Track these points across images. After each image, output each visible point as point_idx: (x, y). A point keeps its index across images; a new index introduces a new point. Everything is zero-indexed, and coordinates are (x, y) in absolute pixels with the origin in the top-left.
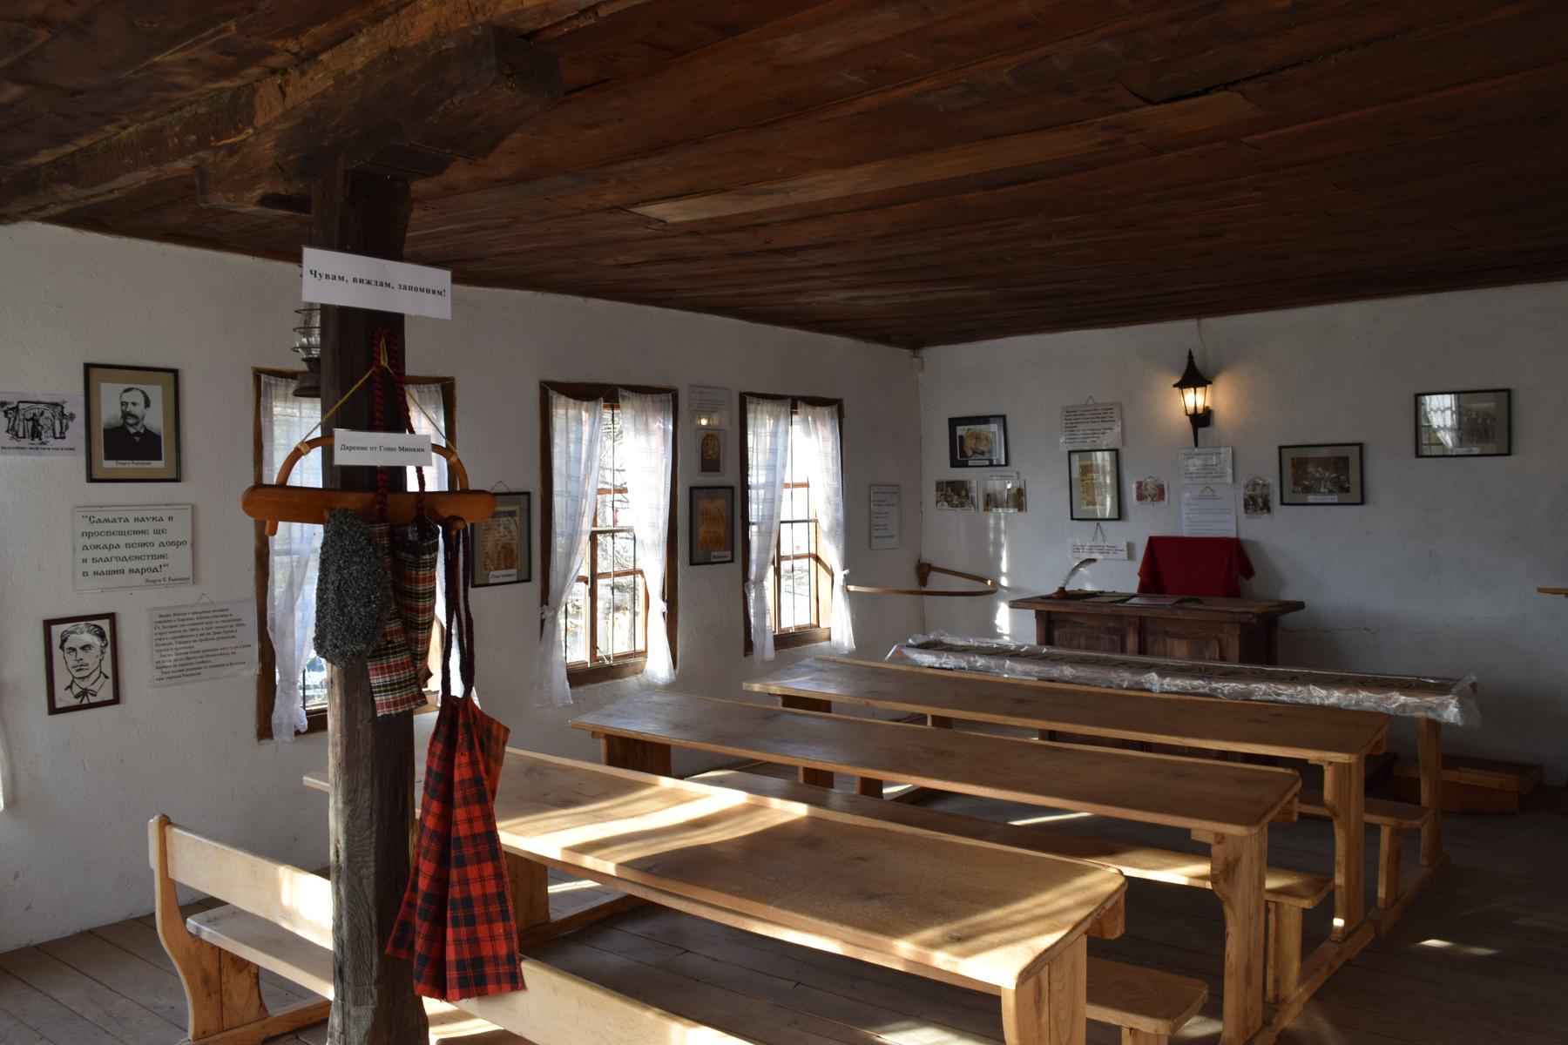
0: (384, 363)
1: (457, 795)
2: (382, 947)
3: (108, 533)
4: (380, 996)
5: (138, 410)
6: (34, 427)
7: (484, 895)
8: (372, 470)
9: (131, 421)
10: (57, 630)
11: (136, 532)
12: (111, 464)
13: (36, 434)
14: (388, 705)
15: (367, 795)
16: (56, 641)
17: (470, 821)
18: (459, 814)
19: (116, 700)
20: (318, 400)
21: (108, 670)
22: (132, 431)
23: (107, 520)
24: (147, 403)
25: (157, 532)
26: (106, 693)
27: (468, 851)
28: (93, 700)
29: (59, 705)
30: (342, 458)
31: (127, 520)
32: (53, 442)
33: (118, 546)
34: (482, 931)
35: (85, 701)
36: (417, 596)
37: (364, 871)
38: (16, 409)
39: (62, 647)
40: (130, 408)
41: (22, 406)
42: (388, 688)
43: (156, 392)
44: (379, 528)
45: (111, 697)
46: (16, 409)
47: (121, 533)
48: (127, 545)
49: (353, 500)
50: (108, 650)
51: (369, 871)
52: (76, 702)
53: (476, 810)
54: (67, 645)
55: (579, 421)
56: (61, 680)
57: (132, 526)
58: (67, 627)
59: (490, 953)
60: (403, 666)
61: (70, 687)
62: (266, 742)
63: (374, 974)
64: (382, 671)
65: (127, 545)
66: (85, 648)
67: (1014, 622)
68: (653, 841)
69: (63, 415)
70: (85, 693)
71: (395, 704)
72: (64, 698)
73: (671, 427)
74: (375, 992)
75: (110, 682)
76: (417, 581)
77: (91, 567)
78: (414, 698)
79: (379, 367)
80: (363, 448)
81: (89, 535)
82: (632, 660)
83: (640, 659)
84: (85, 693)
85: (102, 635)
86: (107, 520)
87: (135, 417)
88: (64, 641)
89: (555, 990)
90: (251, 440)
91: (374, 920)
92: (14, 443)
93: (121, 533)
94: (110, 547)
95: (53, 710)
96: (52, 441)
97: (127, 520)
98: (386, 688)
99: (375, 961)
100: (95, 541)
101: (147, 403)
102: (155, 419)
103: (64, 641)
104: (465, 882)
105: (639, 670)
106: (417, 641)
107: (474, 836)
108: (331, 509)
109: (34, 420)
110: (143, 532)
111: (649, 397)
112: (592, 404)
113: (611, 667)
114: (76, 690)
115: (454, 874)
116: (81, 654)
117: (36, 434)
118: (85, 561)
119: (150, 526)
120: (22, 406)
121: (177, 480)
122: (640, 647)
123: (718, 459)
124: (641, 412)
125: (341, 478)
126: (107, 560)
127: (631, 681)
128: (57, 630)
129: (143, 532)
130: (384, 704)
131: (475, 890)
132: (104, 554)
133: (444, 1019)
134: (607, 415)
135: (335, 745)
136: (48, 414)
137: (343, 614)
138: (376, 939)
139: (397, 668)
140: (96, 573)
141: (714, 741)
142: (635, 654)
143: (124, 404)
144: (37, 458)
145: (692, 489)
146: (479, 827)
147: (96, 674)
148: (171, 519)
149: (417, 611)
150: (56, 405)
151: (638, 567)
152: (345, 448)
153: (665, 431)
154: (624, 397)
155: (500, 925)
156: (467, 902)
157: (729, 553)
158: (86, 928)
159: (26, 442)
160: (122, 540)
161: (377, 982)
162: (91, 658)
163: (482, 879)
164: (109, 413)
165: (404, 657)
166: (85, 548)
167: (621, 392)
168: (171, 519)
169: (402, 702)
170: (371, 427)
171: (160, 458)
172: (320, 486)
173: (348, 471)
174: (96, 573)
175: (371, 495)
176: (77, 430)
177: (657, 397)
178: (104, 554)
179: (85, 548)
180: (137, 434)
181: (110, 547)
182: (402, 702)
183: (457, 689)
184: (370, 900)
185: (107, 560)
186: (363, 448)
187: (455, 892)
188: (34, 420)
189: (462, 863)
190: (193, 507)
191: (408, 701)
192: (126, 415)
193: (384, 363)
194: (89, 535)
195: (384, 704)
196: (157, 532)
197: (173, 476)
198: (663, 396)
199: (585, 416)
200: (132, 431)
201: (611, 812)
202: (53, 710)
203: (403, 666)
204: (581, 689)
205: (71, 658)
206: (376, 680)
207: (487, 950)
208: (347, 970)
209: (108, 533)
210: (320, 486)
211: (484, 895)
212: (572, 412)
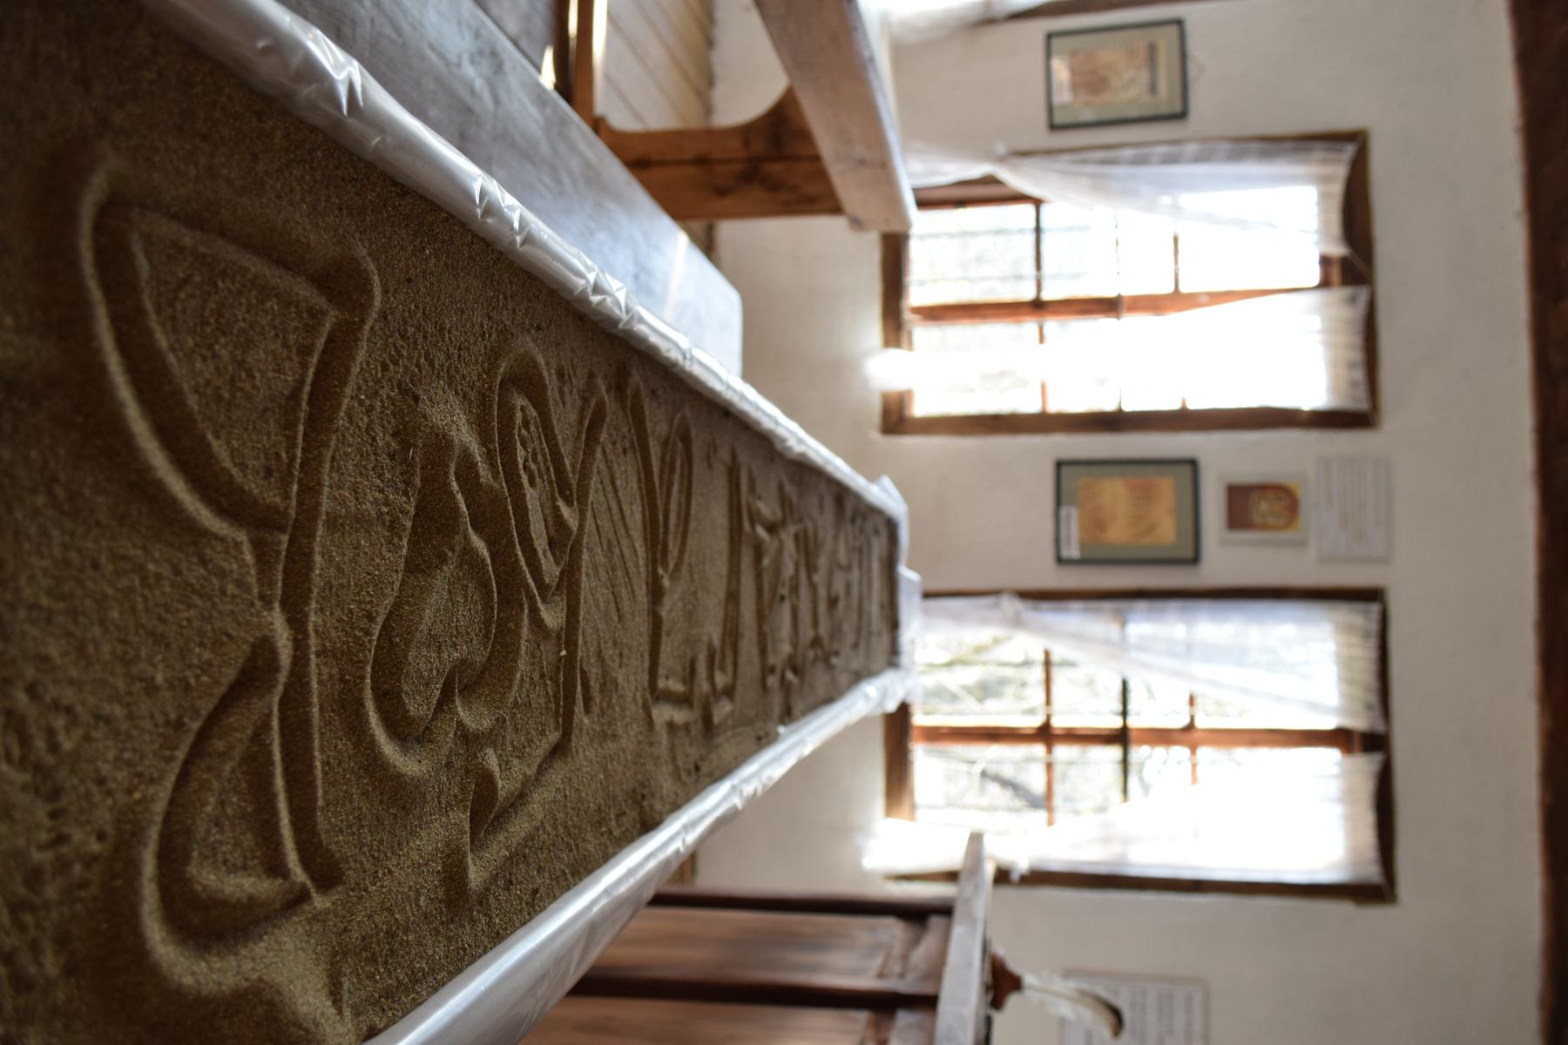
154: (1352, 300)
167: (1363, 294)
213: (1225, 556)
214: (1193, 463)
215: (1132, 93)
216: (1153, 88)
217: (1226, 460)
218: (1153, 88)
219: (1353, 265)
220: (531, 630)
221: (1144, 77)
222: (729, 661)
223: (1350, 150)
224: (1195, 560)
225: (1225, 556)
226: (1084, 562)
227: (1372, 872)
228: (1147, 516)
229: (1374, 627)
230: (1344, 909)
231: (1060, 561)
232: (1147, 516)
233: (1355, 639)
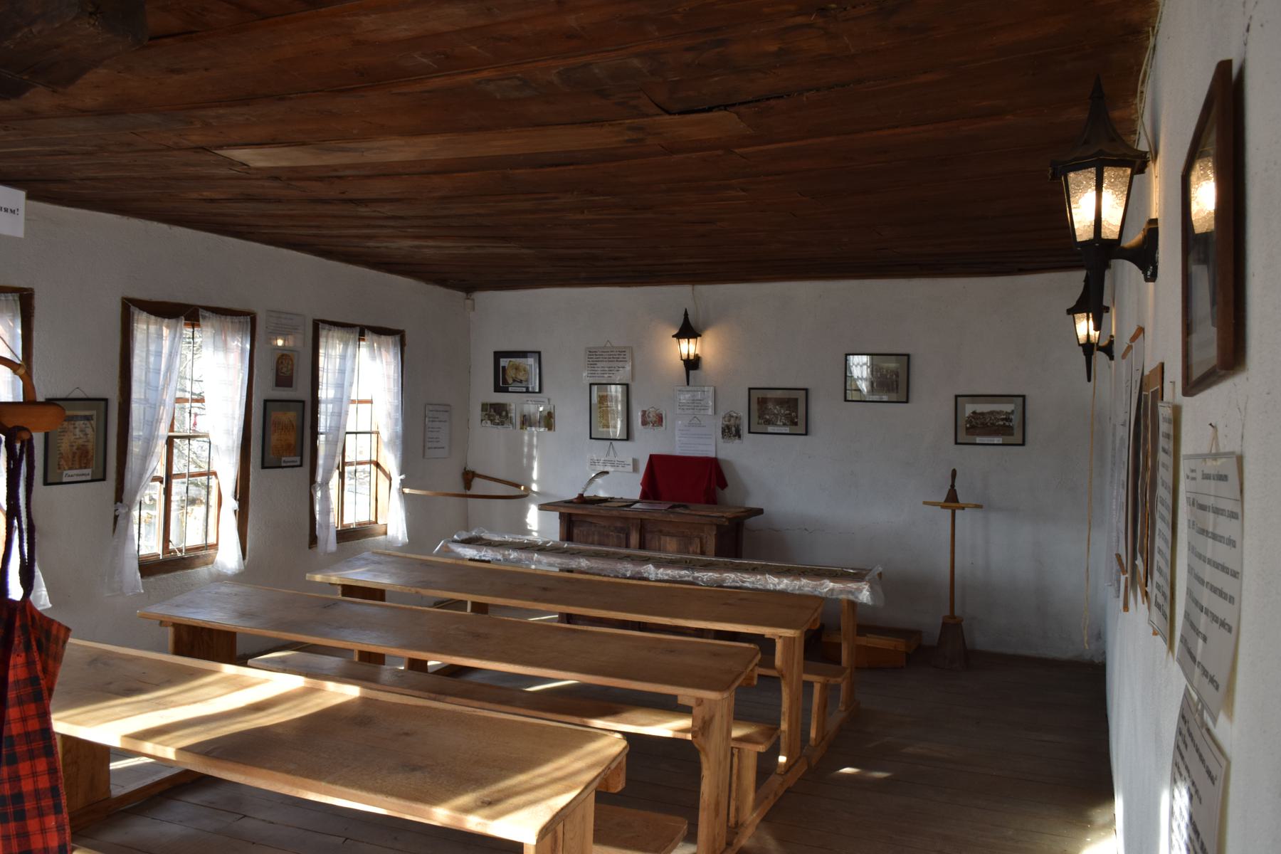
27: (21, 749)
53: (31, 709)
55: (160, 336)
73: (248, 346)
82: (203, 552)
83: (211, 552)
105: (209, 561)
107: (27, 734)
111: (229, 318)
112: (173, 321)
113: (182, 558)
127: (202, 572)
134: (188, 331)
141: (277, 628)
142: (207, 547)
146: (34, 725)
153: (243, 350)
154: (204, 317)
157: (298, 459)
163: (34, 774)
167: (201, 312)
177: (236, 319)
199: (166, 332)
204: (152, 579)
212: (153, 328)
213: (300, 391)
214: (266, 401)
215: (89, 431)
216: (88, 418)
217: (267, 389)
218: (88, 418)
219: (186, 313)
220: (270, 639)
221: (80, 423)
222: (1118, 442)
223: (133, 308)
224: (303, 402)
225: (300, 391)
226: (302, 456)
227: (398, 338)
228: (284, 432)
229: (327, 326)
230: (406, 348)
231: (301, 466)
232: (284, 432)
233: (330, 341)
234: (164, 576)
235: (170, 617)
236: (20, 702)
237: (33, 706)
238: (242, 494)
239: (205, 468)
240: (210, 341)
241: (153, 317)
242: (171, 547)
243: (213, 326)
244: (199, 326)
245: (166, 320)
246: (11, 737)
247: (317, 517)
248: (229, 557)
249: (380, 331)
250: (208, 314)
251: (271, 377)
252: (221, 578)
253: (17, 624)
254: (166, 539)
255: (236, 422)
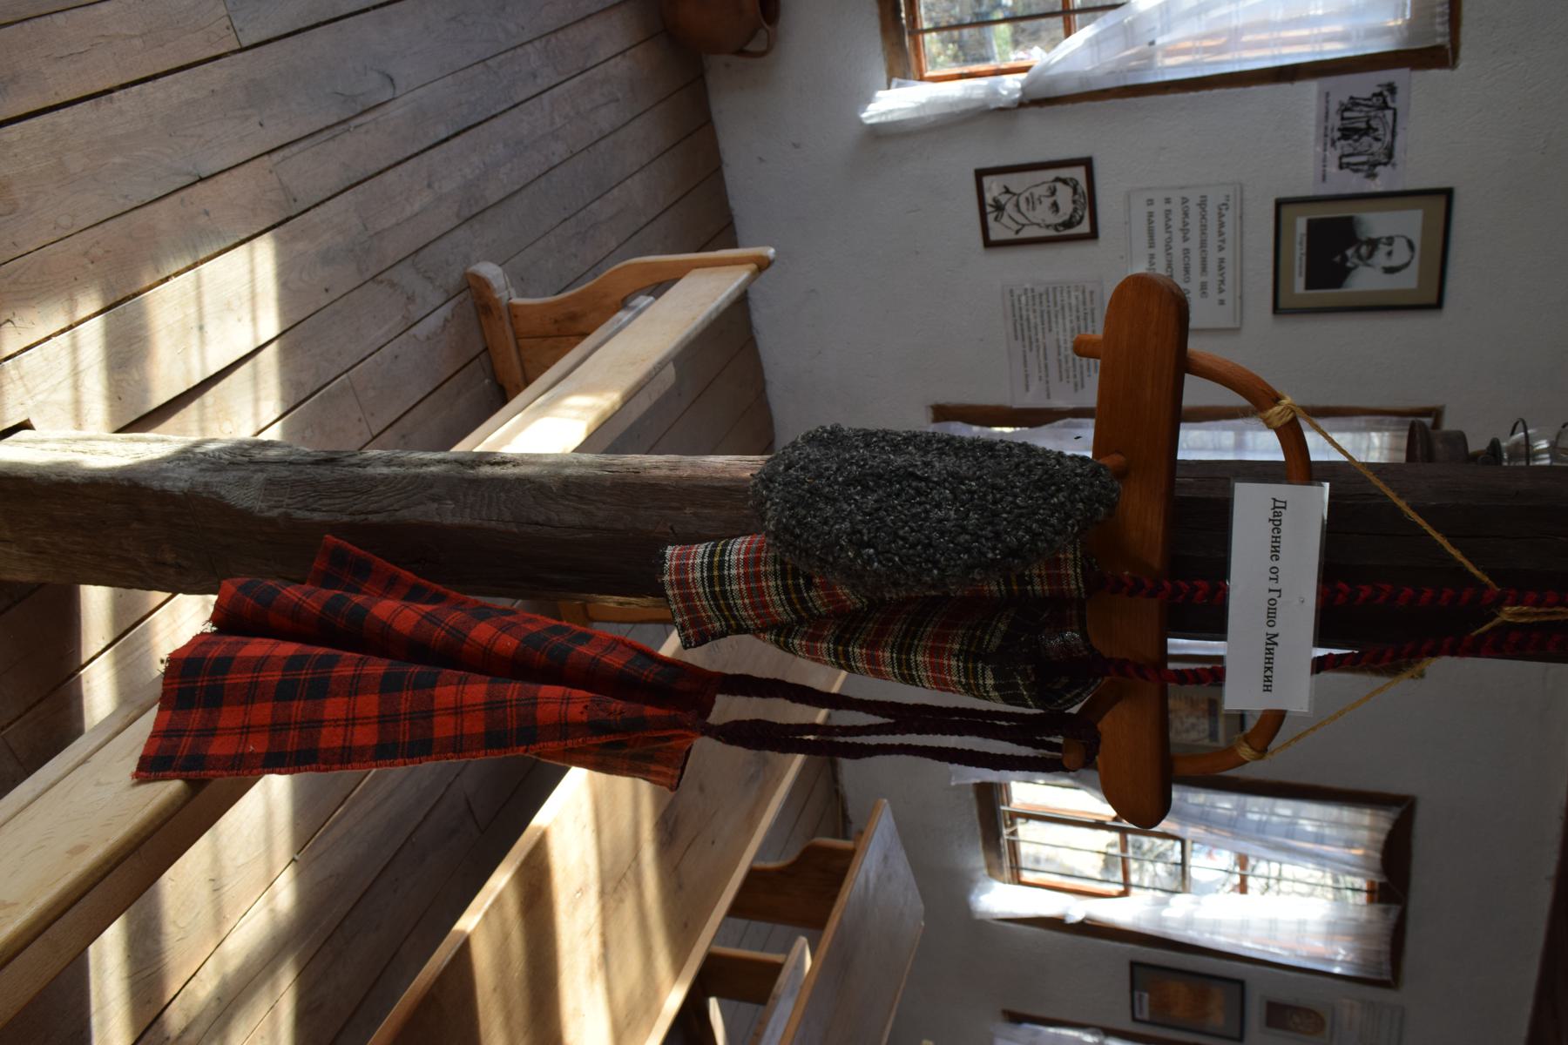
0: (1507, 613)
1: (513, 690)
2: (334, 528)
3: (1204, 228)
4: (271, 521)
5: (1380, 258)
6: (1356, 131)
7: (320, 723)
8: (1220, 568)
9: (1364, 250)
10: (1079, 173)
11: (1204, 261)
12: (1301, 226)
13: (1347, 133)
14: (681, 569)
15: (570, 518)
16: (1065, 173)
17: (458, 710)
18: (478, 690)
19: (989, 244)
20: (1401, 457)
21: (1027, 233)
22: (1350, 252)
23: (1222, 225)
24: (1390, 270)
25: (1204, 286)
26: (997, 233)
27: (405, 701)
28: (991, 218)
29: (987, 180)
30: (1249, 501)
31: (1221, 249)
32: (1333, 155)
33: (1185, 239)
34: (262, 712)
35: (989, 209)
36: (904, 649)
37: (450, 505)
38: (1385, 106)
39: (1058, 179)
40: (1383, 249)
41: (1389, 114)
42: (716, 570)
43: (1407, 281)
44: (1073, 580)
45: (993, 236)
46: (1385, 106)
47: (1203, 244)
48: (1186, 251)
49: (1144, 520)
50: (1051, 233)
51: (449, 515)
52: (989, 198)
53: (475, 725)
54: (1059, 185)
55: (1349, 844)
56: (1016, 181)
57: (1213, 257)
58: (1083, 185)
59: (221, 724)
60: (760, 606)
61: (1007, 191)
62: (930, 415)
63: (300, 514)
64: (752, 561)
65: (1186, 251)
66: (1055, 206)
67: (1253, 821)
68: (519, 997)
69: (1375, 165)
70: (999, 207)
71: (682, 584)
72: (993, 186)
73: (1337, 970)
74: (275, 513)
75: (1010, 235)
76: (935, 652)
77: (1159, 209)
78: (696, 622)
79: (1500, 602)
80: (1275, 558)
81: (1203, 204)
82: (1006, 863)
83: (1007, 874)
84: (999, 207)
85: (1068, 224)
86: (1222, 225)
87: (1370, 255)
88: (1065, 182)
89: (80, 849)
90: (1332, 403)
91: (374, 518)
92: (1334, 107)
93: (1203, 244)
94: (1185, 230)
95: (980, 174)
96: (1338, 153)
97: (1221, 249)
98: (716, 567)
99: (317, 516)
100: (1194, 211)
101: (1390, 270)
102: (1366, 280)
103: (1065, 182)
104: (354, 688)
105: (994, 871)
106: (814, 638)
107: (429, 714)
108: (1121, 474)
109: (1369, 130)
110: (1204, 269)
111: (1386, 948)
112: (1378, 866)
113: (999, 835)
114: (1003, 199)
115: (378, 667)
116: (1048, 202)
117: (1347, 133)
118: (1168, 201)
119: (1212, 277)
120: (1389, 114)
121: (1276, 309)
122: (1027, 876)
123: (1284, 1027)
124: (1360, 933)
125: (1204, 505)
126: (1168, 227)
127: (977, 860)
128: (1079, 173)
129: (1204, 269)
130: (686, 560)
131: (334, 707)
132: (1176, 222)
133: (127, 628)
134: (1360, 883)
135: (674, 467)
136: (1377, 146)
137: (848, 483)
138: (346, 519)
139: (756, 593)
140: (1151, 214)
141: (1413, 508)
142: (1016, 869)
143: (1390, 241)
144: (1312, 138)
145: (1241, 983)
146: (443, 727)
147: (1022, 220)
148: (1222, 302)
149: (873, 645)
150: (1390, 153)
151: (1134, 891)
152: (1278, 509)
153: (1332, 962)
154: (1386, 911)
155: (263, 749)
156: (320, 690)
157: (1146, 1016)
158: (737, 222)
159: (1336, 121)
160: (1194, 244)
161: (287, 516)
162: (1043, 213)
163: (351, 721)
164: (1376, 223)
165: (780, 610)
166: (1185, 200)
167: (1395, 910)
168: (1222, 302)
169: (687, 598)
170: (1332, 572)
171: (1309, 286)
172: (1182, 455)
173: (1219, 516)
174: (1151, 214)
175: (1156, 561)
176: (1354, 183)
177: (1385, 958)
178: (1176, 222)
179: (1185, 200)
180: (1345, 259)
181: (1185, 230)
182: (687, 598)
183: (727, 709)
184: (405, 514)
185: (1168, 227)
186: (1275, 558)
187: (347, 664)
188: (1369, 130)
189: (389, 685)
190: (1235, 331)
191: (691, 610)
192: (1373, 244)
193: (1507, 613)
194: (1203, 204)
195: (686, 560)
196: (1204, 286)
197: (1282, 304)
198: (1386, 967)
199: (1359, 852)
200: (1350, 252)
201: (629, 907)
202: (980, 174)
203: (760, 606)
204: (972, 795)
205: (1042, 191)
206: (738, 548)
207: (229, 717)
208: (324, 472)
209: (1204, 228)
210: (1182, 455)
211: (320, 723)
212: (1364, 835)
215: (1193, 735)
216: (1213, 735)
234: (975, 812)
235: (865, 849)
236: (492, 705)
237: (480, 728)
238: (1088, 928)
239: (1134, 879)
240: (1351, 914)
241: (1382, 837)
242: (1019, 821)
243: (1370, 922)
244: (1371, 900)
245: (1378, 856)
246: (433, 685)
247: (1051, 1030)
248: (998, 899)
249: (1397, 938)
250: (1393, 915)
251: (1284, 996)
252: (956, 891)
253: (649, 711)
254: (1029, 817)
255: (1207, 936)
